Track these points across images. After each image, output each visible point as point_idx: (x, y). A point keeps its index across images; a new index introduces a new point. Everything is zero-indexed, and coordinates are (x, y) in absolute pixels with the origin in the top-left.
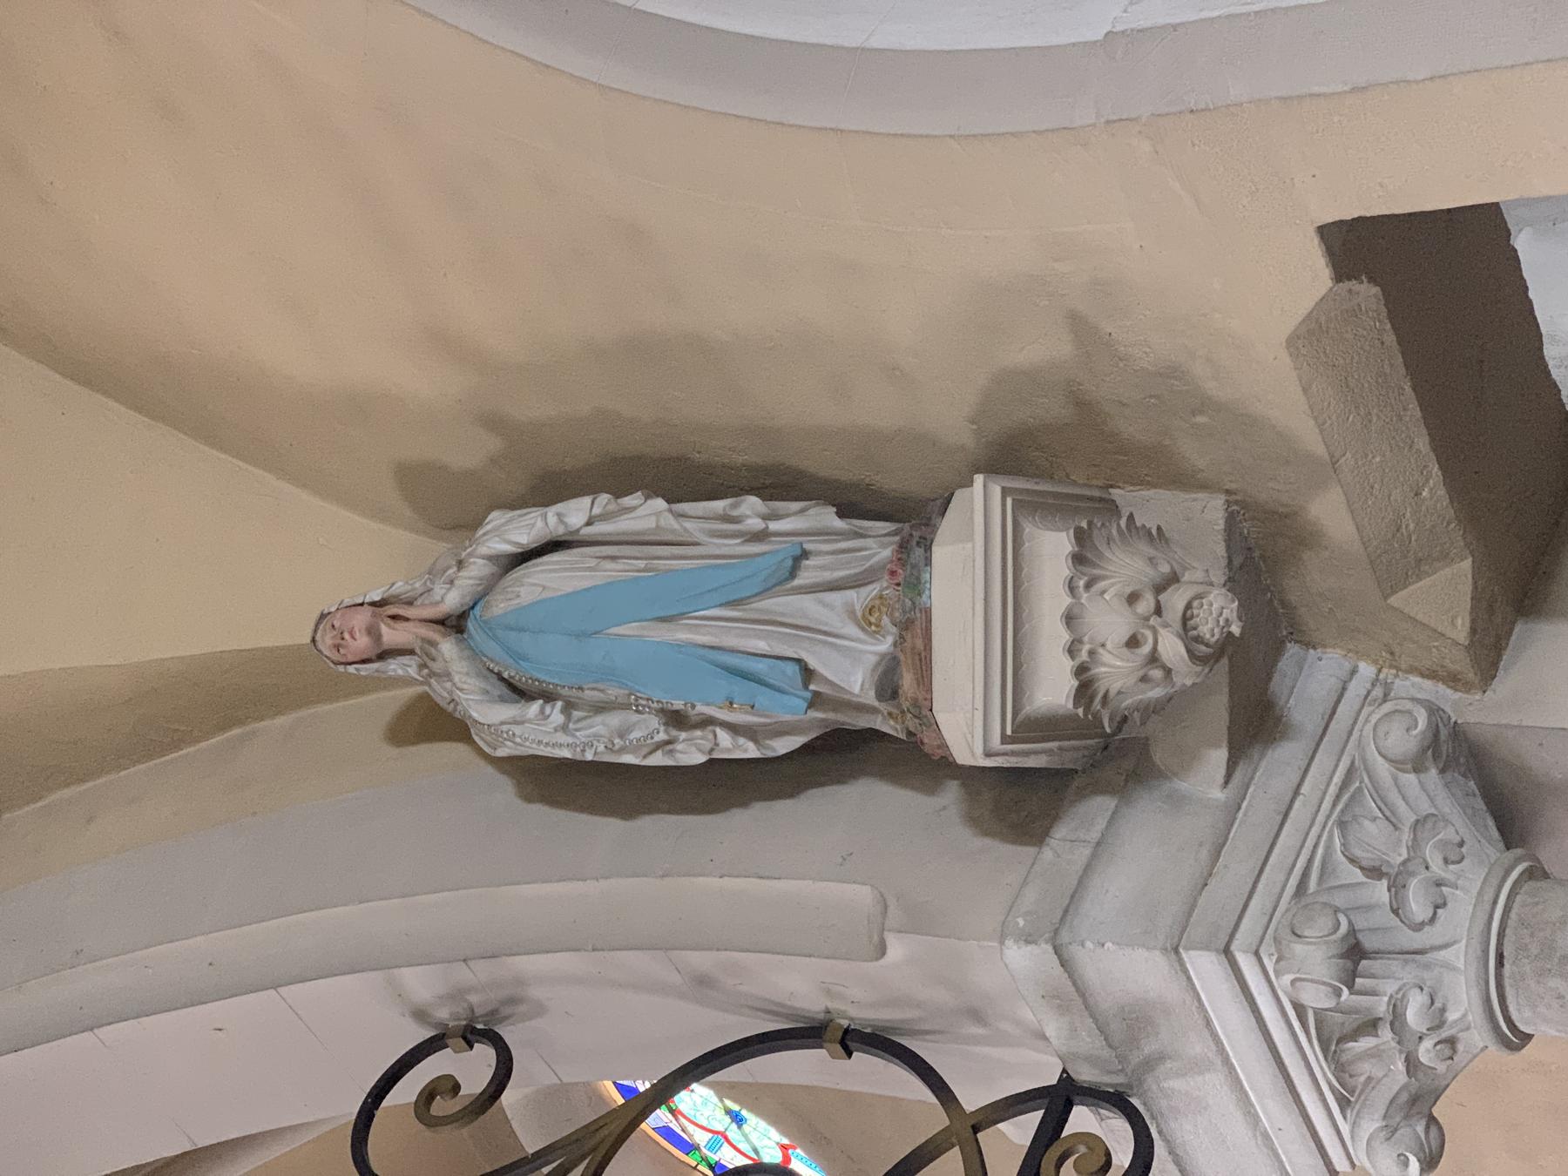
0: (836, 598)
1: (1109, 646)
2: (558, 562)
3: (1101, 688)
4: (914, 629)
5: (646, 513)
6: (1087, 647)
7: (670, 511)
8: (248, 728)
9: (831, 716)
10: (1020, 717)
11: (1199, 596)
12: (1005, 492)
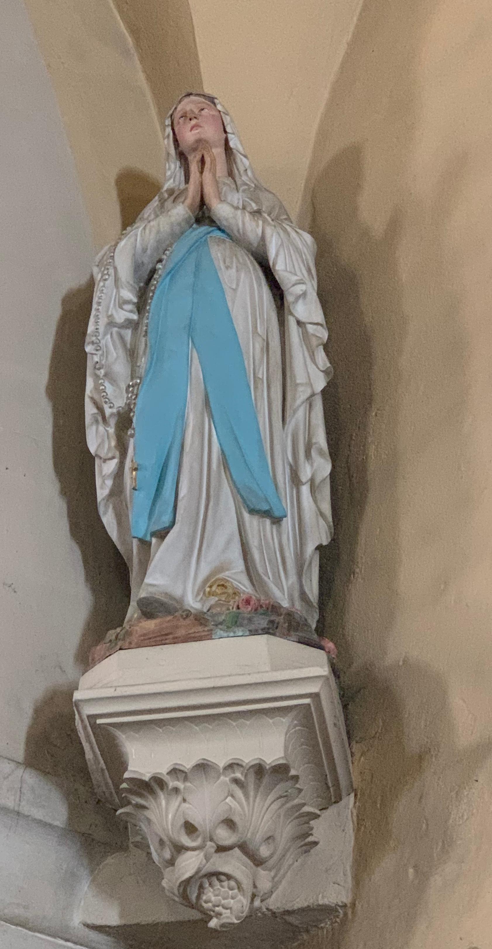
0: (235, 553)
1: (185, 805)
2: (261, 297)
3: (149, 802)
4: (198, 626)
5: (311, 373)
6: (180, 785)
7: (313, 395)
8: (133, 51)
9: (135, 560)
10: (112, 729)
11: (239, 887)
12: (315, 696)
